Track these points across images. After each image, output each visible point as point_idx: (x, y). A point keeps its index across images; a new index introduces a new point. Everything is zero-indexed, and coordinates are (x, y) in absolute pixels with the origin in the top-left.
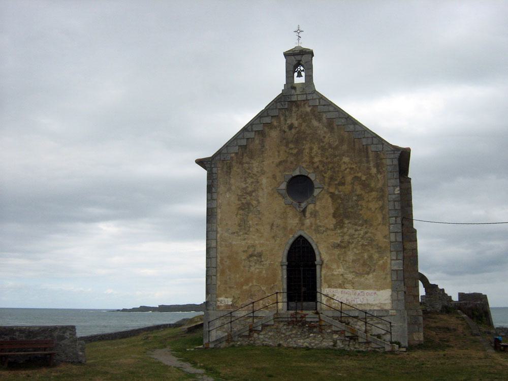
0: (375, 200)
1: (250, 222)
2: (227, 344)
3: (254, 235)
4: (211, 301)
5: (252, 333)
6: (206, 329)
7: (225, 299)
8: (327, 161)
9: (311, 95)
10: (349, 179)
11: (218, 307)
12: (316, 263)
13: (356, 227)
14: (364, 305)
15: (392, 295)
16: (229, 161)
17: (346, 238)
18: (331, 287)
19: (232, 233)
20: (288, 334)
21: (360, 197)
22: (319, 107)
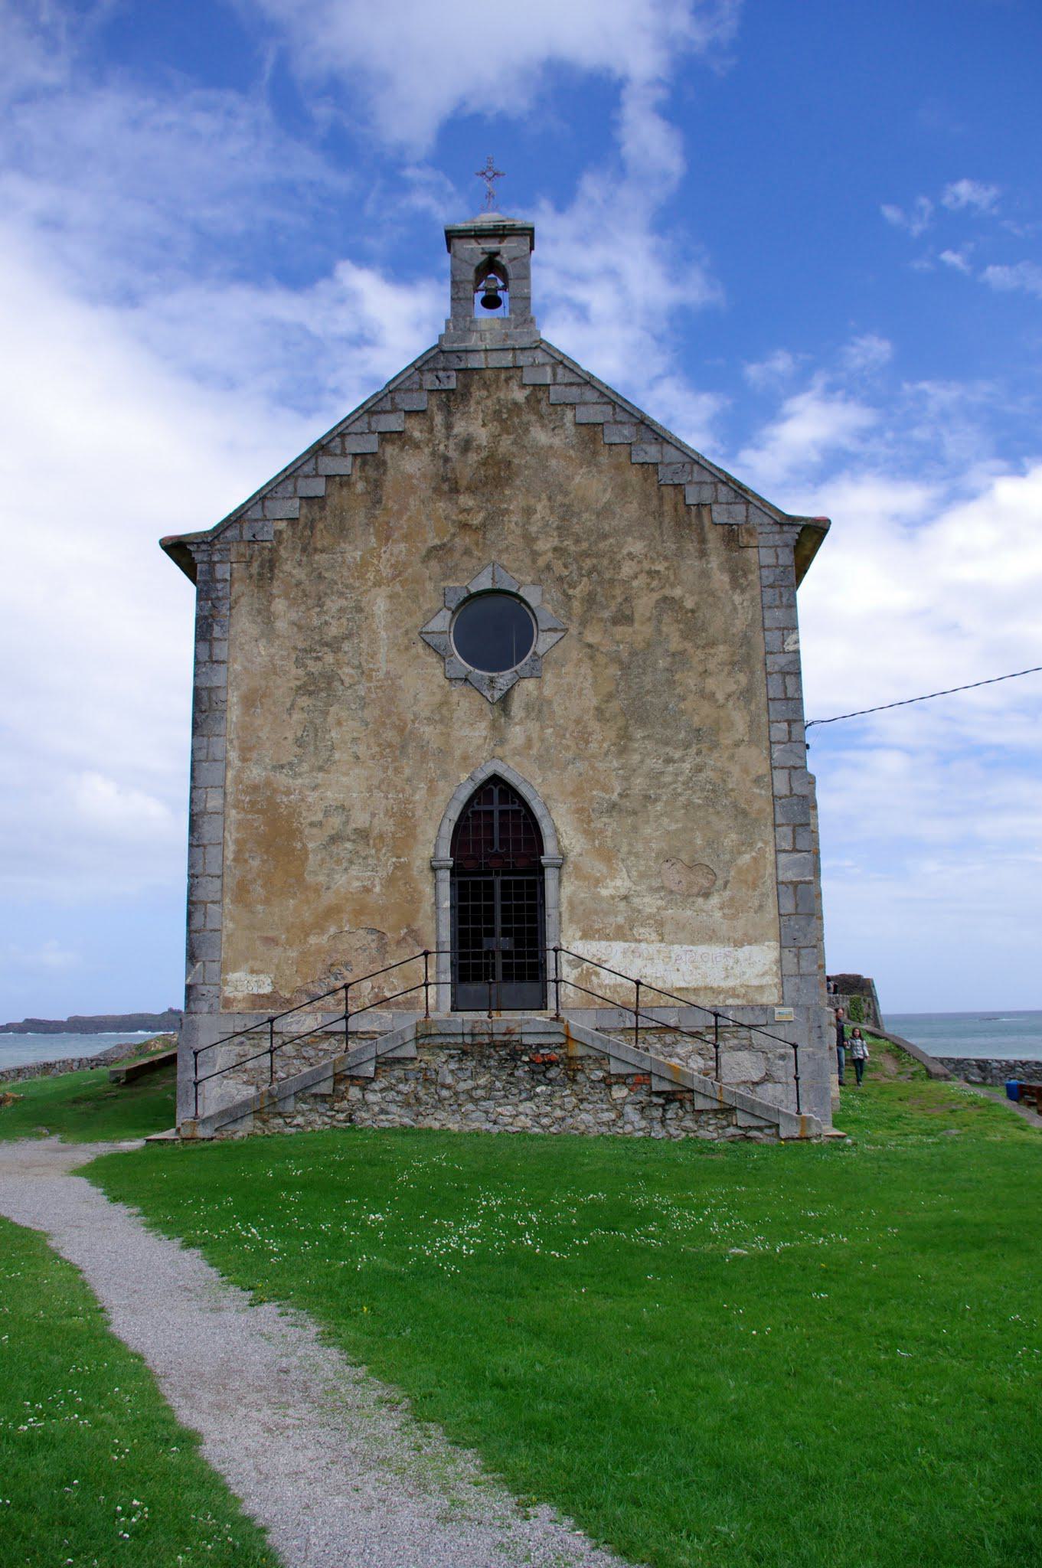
0: (726, 669)
1: (333, 734)
2: (259, 1124)
3: (347, 774)
4: (204, 984)
5: (342, 1087)
6: (184, 1074)
7: (249, 977)
8: (578, 549)
9: (527, 353)
10: (644, 604)
11: (227, 1002)
12: (544, 860)
13: (668, 749)
14: (696, 990)
15: (780, 961)
16: (269, 544)
17: (639, 783)
18: (592, 938)
19: (274, 768)
20: (463, 1086)
21: (679, 658)
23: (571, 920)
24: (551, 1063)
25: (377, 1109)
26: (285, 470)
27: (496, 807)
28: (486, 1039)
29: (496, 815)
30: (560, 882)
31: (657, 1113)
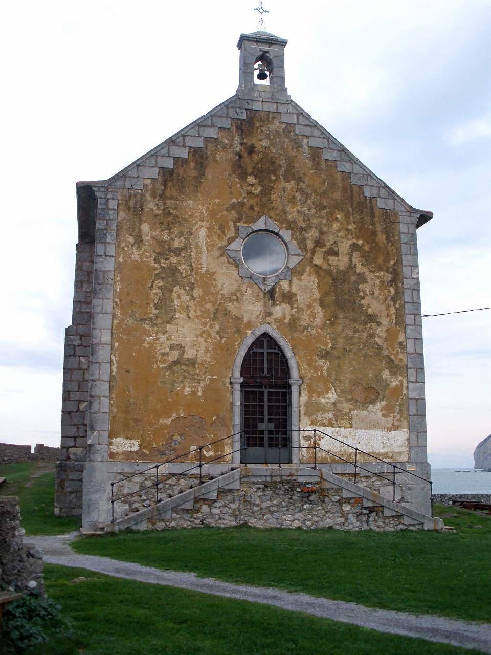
5: (198, 505)
7: (125, 441)
9: (284, 106)
12: (292, 381)
15: (409, 439)
20: (265, 505)
22: (296, 126)
23: (305, 414)
24: (313, 492)
25: (217, 517)
26: (151, 151)
27: (265, 350)
28: (278, 479)
29: (266, 354)
30: (300, 393)
31: (365, 518)
